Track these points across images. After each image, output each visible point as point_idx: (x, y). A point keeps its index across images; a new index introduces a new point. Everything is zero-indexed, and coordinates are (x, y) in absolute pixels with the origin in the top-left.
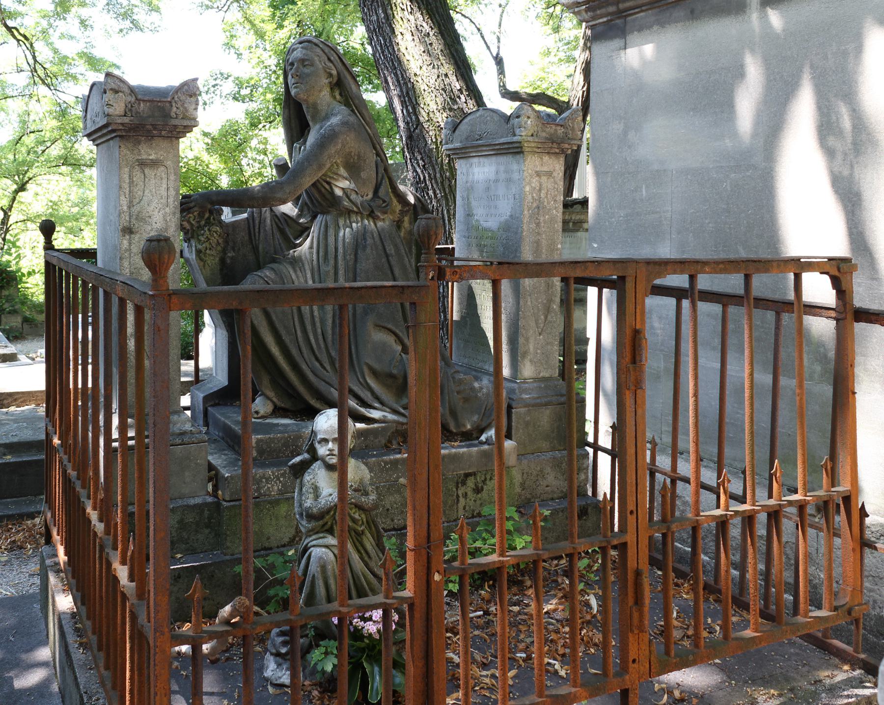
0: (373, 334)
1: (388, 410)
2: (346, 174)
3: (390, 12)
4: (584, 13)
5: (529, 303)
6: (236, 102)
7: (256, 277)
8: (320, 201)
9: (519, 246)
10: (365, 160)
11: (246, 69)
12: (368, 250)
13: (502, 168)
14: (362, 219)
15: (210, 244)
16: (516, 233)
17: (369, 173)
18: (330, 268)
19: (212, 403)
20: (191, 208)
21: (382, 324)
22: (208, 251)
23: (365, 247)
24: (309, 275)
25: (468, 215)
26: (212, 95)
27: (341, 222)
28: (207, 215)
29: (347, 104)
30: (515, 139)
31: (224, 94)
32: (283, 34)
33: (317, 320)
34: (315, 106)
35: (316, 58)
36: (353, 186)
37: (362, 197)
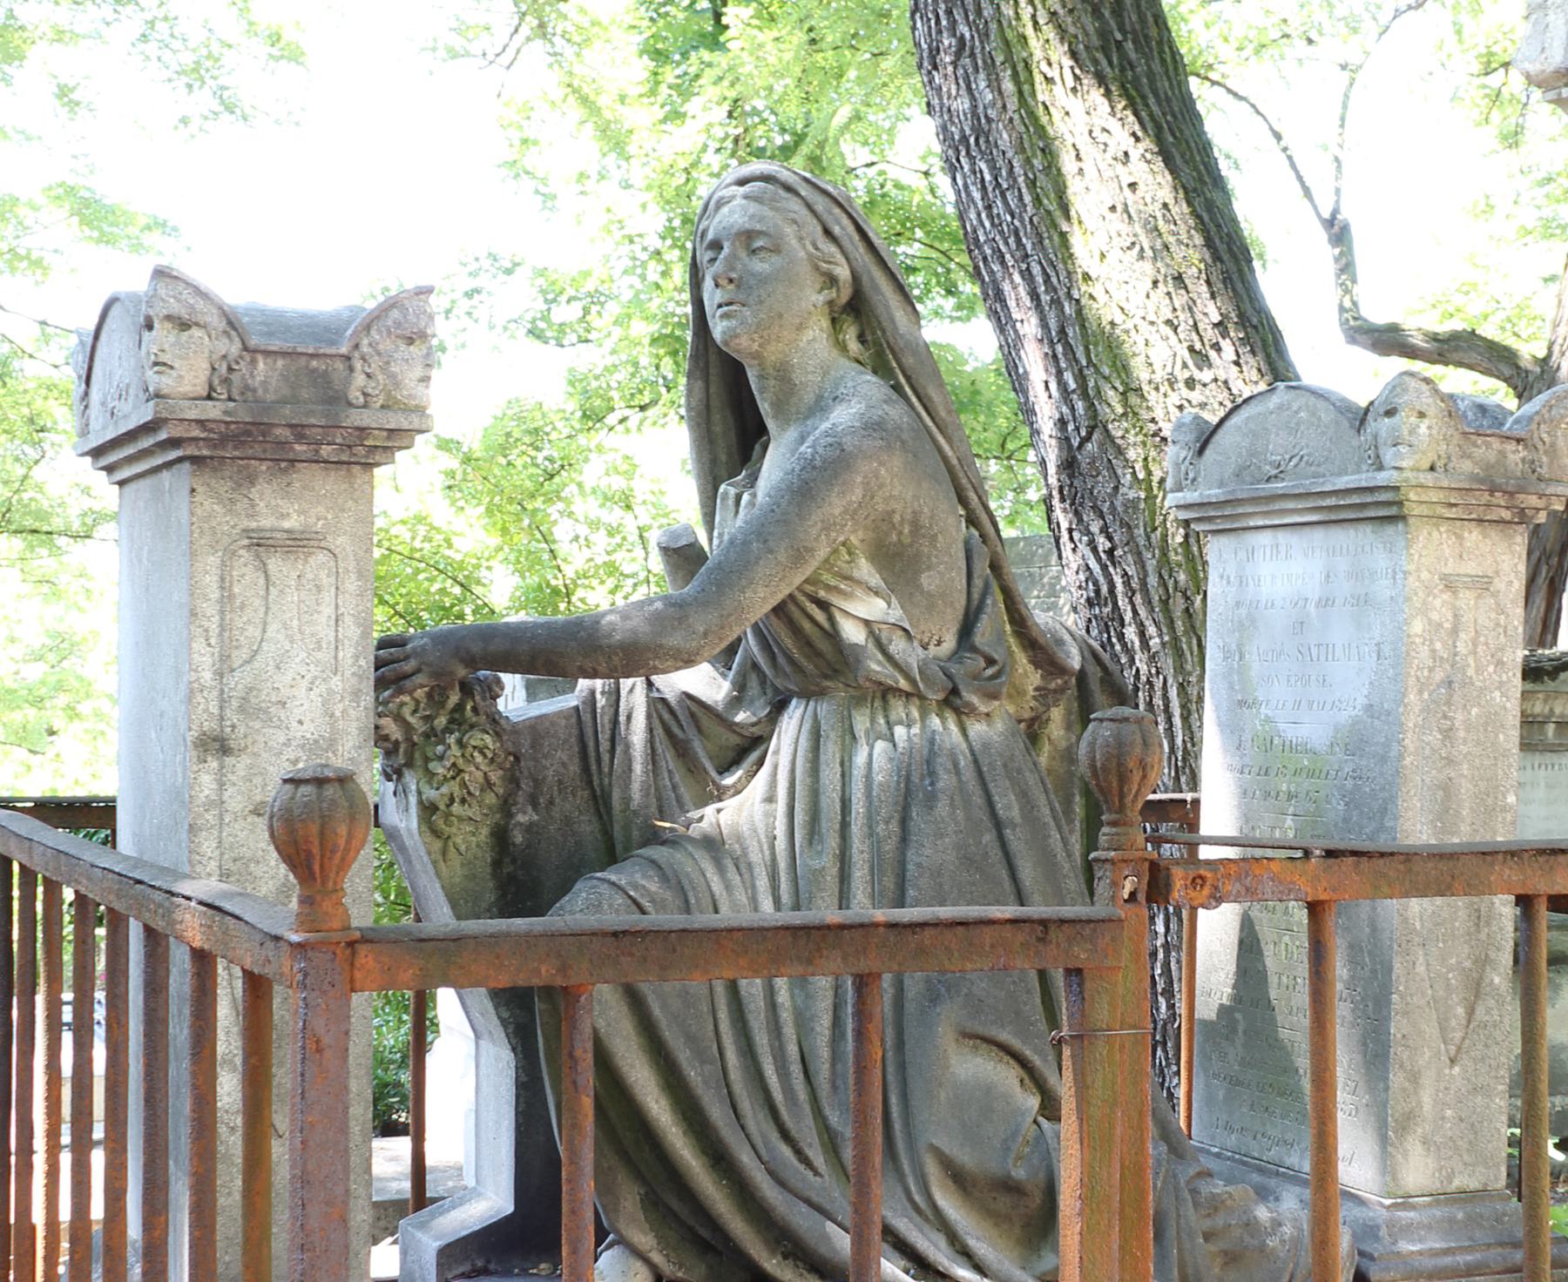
2: (875, 580)
5: (1421, 969)
7: (604, 889)
8: (801, 659)
9: (1392, 799)
10: (934, 538)
12: (942, 808)
13: (1342, 565)
15: (464, 785)
16: (1384, 759)
17: (945, 576)
21: (980, 1030)
23: (931, 799)
27: (861, 722)
28: (454, 698)
30: (1382, 478)
33: (786, 1016)
34: (783, 375)
35: (789, 230)
36: (896, 614)
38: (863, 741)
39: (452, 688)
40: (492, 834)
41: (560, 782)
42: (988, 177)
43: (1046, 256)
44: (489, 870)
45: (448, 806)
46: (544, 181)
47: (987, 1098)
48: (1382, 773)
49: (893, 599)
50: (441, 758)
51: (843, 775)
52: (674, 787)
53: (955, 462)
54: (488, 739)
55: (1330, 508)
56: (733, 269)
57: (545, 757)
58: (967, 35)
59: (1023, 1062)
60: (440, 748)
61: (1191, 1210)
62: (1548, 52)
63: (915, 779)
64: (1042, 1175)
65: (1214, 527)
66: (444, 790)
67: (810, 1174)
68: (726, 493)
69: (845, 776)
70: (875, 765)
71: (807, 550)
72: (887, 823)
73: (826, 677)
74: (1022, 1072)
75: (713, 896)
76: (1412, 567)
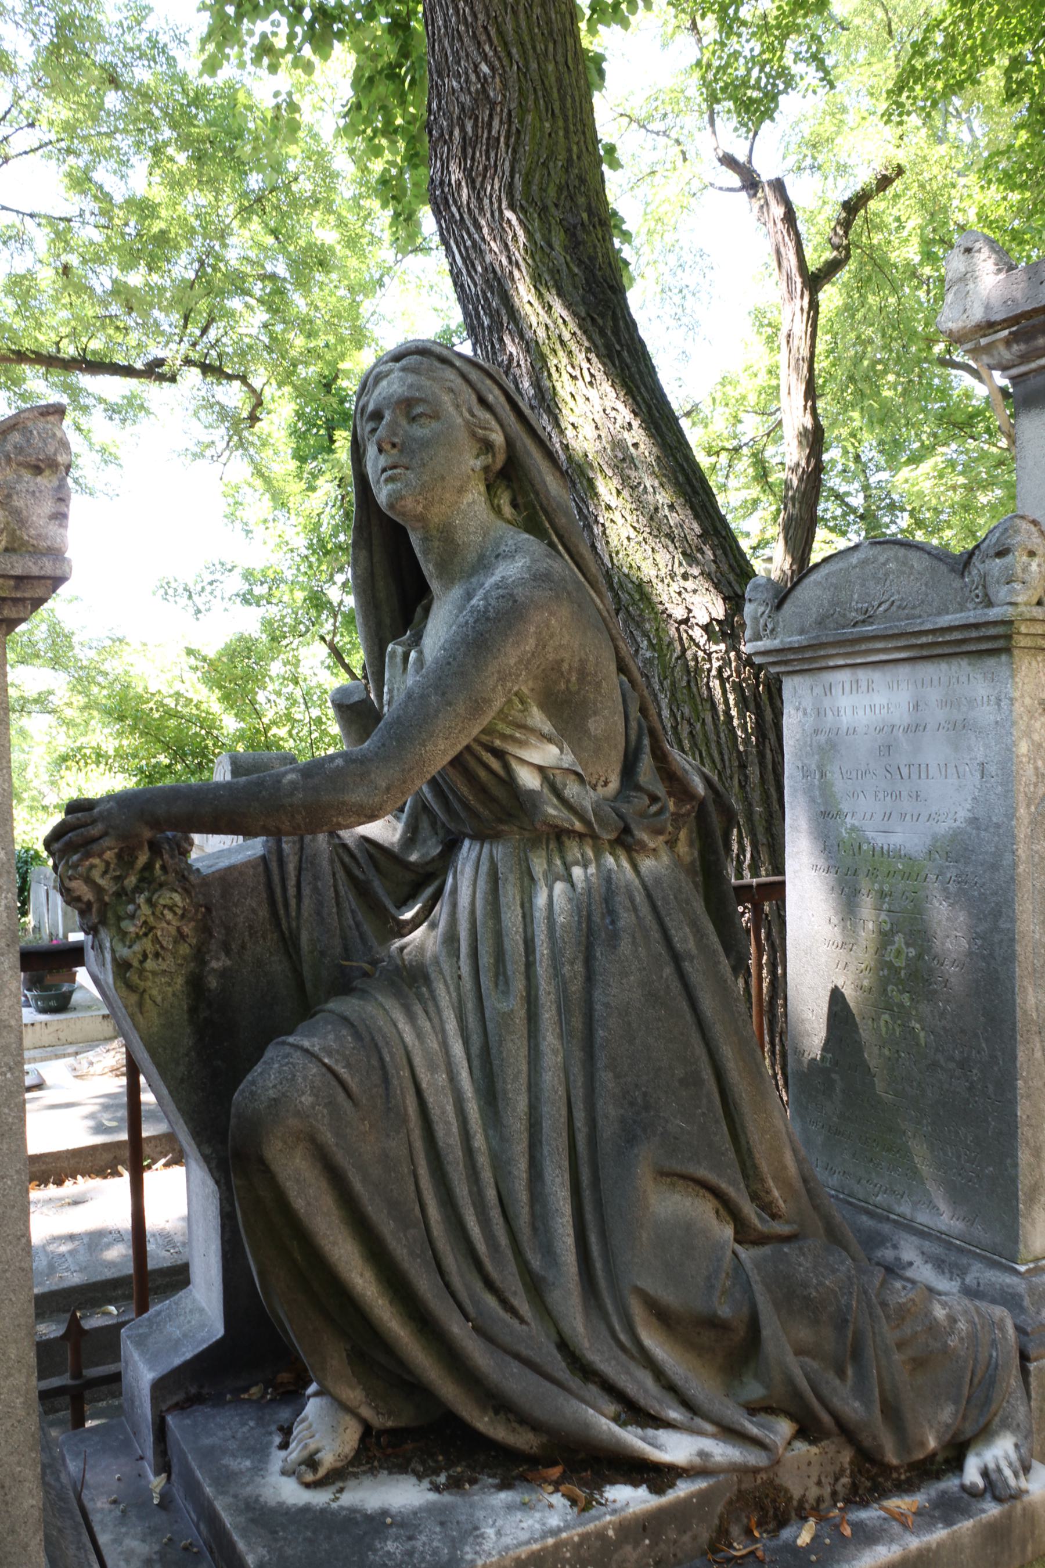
0: (653, 1199)
1: (709, 1428)
2: (547, 727)
3: (548, 383)
4: (1002, 348)
6: (247, 607)
7: (297, 1057)
8: (477, 803)
9: (1010, 903)
10: (598, 685)
12: (625, 947)
13: (933, 695)
14: (598, 855)
15: (156, 940)
16: (995, 867)
17: (608, 722)
18: (515, 1004)
19: (179, 1397)
20: (94, 840)
21: (679, 1168)
22: (150, 964)
23: (614, 937)
24: (452, 1026)
25: (824, 814)
27: (538, 865)
28: (143, 858)
29: (532, 525)
30: (994, 613)
31: (227, 595)
33: (483, 1160)
34: (447, 535)
35: (446, 398)
36: (568, 759)
37: (594, 787)
38: (542, 883)
39: (140, 847)
40: (187, 982)
41: (251, 927)
43: (579, 495)
44: (186, 1016)
45: (141, 962)
46: (246, 524)
47: (684, 1237)
48: (992, 880)
49: (565, 745)
50: (132, 917)
51: (524, 917)
52: (358, 925)
54: (177, 897)
55: (922, 646)
56: (395, 434)
57: (236, 905)
60: (131, 908)
62: (969, 312)
63: (597, 918)
64: (745, 1310)
65: (790, 669)
66: (137, 948)
67: (515, 1323)
68: (394, 652)
69: (527, 917)
70: (556, 908)
72: (572, 964)
73: (501, 821)
75: (405, 1047)
76: (1017, 694)
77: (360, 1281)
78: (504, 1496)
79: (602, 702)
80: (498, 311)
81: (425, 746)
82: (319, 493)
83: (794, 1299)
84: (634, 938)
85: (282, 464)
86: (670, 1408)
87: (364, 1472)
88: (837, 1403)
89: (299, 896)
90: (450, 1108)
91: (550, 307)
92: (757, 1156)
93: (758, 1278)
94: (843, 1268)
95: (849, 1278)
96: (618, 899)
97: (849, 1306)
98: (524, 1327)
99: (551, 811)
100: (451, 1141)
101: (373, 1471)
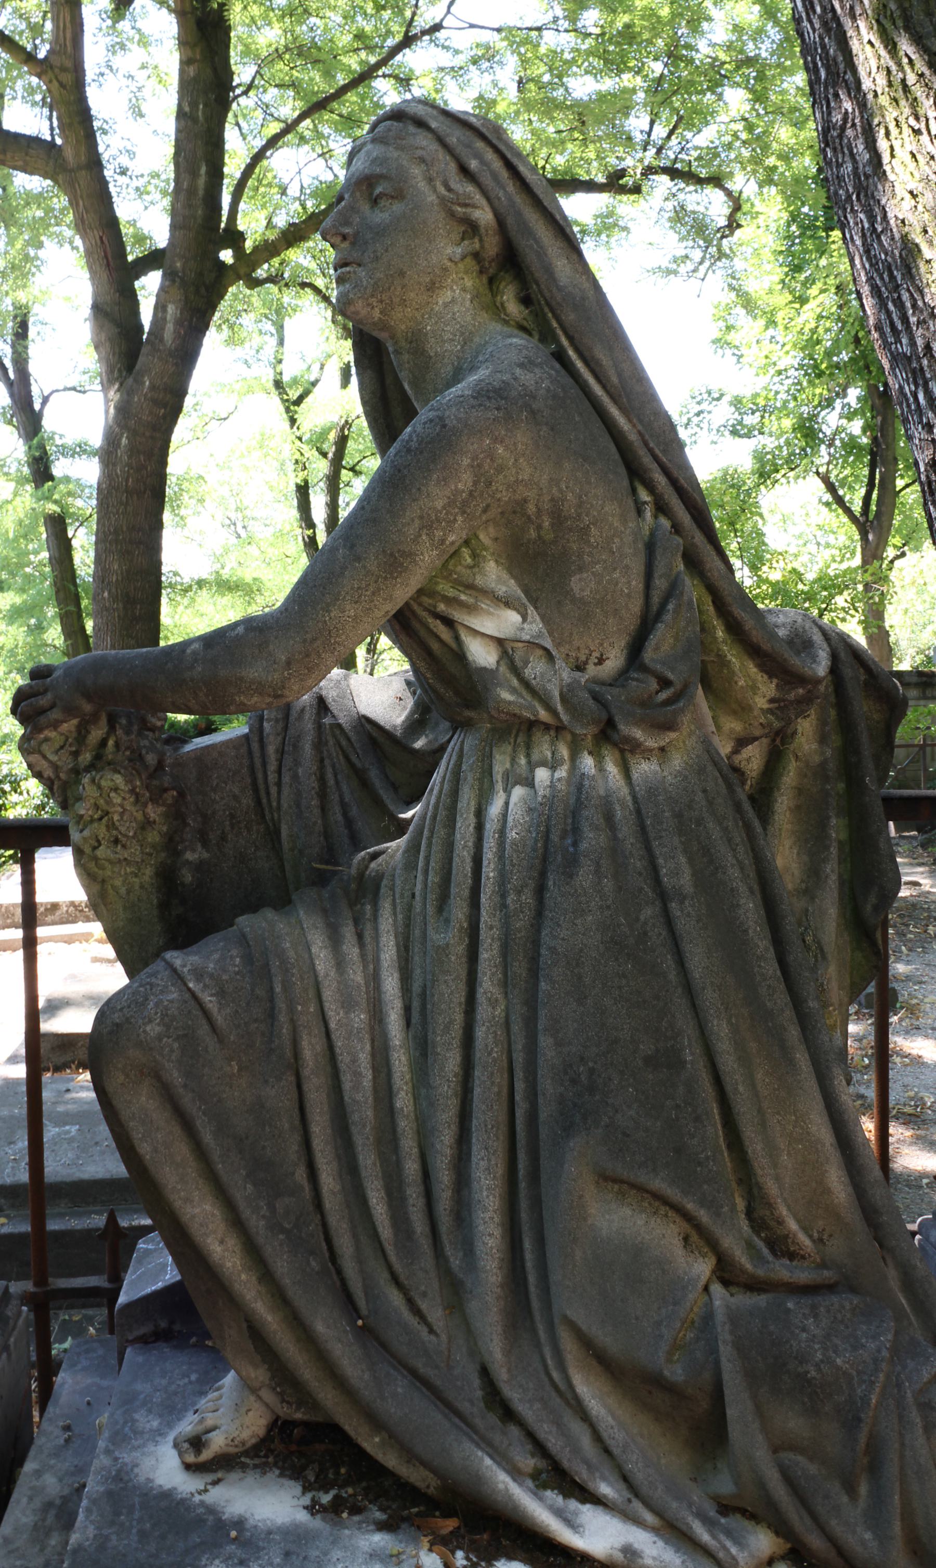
0: (594, 1208)
1: (649, 1517)
2: (507, 586)
10: (584, 532)
11: (747, 382)
12: (584, 877)
15: (111, 826)
17: (612, 574)
23: (571, 863)
24: (389, 954)
26: (697, 429)
31: (715, 427)
32: (808, 315)
33: (406, 1126)
35: (416, 171)
36: (535, 627)
37: (580, 667)
41: (232, 816)
42: (866, 225)
44: (155, 912)
49: (531, 610)
53: (633, 437)
56: (347, 223)
58: (850, 110)
59: (687, 1217)
61: (921, 1440)
63: (555, 837)
69: (480, 828)
70: (510, 819)
71: (403, 554)
72: (519, 892)
74: (686, 1225)
77: (219, 1249)
78: (379, 1539)
79: (590, 554)
80: (835, 60)
81: (329, 611)
82: (812, 304)
83: (776, 1371)
84: (598, 865)
85: (764, 275)
86: (604, 1479)
87: (256, 1467)
88: (836, 1526)
89: (279, 784)
90: (364, 1057)
91: (895, 45)
92: (759, 1172)
93: (728, 1337)
94: (872, 1345)
95: (876, 1361)
96: (585, 813)
97: (865, 1400)
98: (433, 1338)
99: (506, 695)
100: (359, 1097)
101: (263, 1468)
